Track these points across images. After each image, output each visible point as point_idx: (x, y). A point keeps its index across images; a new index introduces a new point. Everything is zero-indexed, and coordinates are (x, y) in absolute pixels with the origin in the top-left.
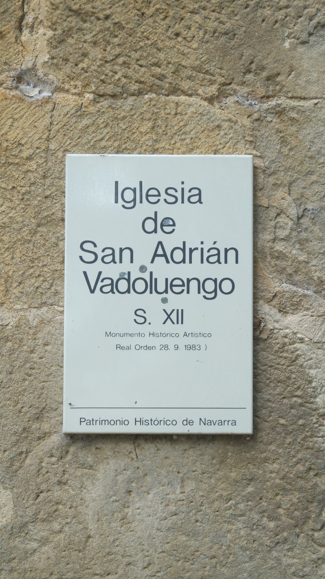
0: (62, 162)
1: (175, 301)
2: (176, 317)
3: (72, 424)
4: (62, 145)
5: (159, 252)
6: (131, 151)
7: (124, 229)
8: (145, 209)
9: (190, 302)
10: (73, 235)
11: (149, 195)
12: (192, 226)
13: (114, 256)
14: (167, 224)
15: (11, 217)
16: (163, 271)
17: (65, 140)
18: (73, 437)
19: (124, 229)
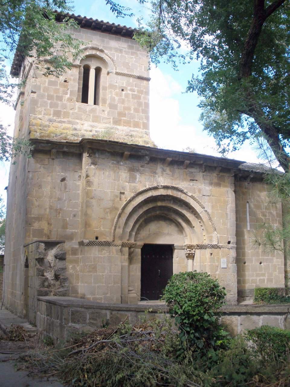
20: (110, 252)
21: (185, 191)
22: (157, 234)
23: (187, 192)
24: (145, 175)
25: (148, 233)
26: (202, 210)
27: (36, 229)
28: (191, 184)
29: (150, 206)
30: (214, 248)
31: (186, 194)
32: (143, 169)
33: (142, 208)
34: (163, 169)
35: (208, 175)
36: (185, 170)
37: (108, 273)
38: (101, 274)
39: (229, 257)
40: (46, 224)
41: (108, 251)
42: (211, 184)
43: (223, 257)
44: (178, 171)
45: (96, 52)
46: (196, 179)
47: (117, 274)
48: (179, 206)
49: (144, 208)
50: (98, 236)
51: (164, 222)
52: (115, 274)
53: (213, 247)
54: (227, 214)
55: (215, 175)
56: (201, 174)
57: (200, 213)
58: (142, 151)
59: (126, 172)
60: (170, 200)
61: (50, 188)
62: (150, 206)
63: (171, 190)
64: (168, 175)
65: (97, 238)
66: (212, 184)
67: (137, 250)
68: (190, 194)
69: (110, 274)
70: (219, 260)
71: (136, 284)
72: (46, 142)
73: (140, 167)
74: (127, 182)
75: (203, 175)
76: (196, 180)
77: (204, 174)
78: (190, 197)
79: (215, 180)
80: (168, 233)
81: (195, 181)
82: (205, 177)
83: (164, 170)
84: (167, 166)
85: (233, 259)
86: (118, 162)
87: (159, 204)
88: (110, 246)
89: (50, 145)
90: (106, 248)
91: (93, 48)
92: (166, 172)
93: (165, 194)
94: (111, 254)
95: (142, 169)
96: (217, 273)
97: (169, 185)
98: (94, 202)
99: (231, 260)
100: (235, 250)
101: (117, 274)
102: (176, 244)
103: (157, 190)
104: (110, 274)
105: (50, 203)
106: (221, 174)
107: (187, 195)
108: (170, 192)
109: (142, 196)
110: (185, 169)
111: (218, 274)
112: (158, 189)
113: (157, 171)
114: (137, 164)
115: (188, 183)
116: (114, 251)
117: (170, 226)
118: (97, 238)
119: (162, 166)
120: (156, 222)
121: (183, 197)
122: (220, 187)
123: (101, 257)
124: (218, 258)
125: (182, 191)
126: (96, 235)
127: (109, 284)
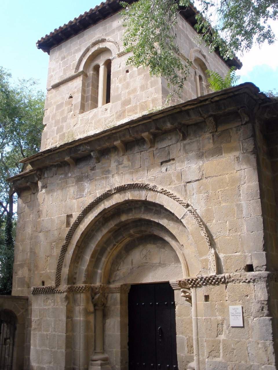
0: (229, 308)
1: (237, 317)
2: (237, 318)
3: (231, 326)
4: (58, 282)
5: (236, 313)
6: (71, 261)
7: (233, 311)
8: (235, 310)
9: (238, 317)
10: (230, 312)
11: (235, 309)
12: (238, 311)
13: (233, 313)
14: (236, 311)
15: (205, 341)
16: (236, 314)
17: (241, 15)
18: (232, 327)
19: (233, 311)
20: (54, 302)
21: (151, 185)
22: (144, 267)
23: (155, 186)
24: (96, 180)
25: (130, 266)
26: (186, 210)
27: (20, 278)
28: (164, 169)
29: (112, 224)
30: (211, 283)
31: (154, 191)
32: (93, 172)
33: (101, 231)
34: (118, 162)
35: (194, 142)
36: (152, 149)
37: (52, 332)
38: (45, 333)
39: (248, 301)
40: (27, 271)
41: (53, 301)
42: (201, 156)
43: (234, 302)
44: (140, 156)
45: (98, 46)
46: (171, 157)
47: (61, 334)
48: (155, 213)
49: (103, 229)
50: (44, 280)
51: (154, 244)
52: (59, 334)
53: (208, 281)
54: (239, 206)
55: (208, 135)
56: (180, 145)
57: (183, 218)
58: (81, 148)
59: (74, 184)
60: (140, 208)
61: (32, 228)
62: (112, 224)
63: (130, 191)
64: (126, 168)
65: (43, 283)
66: (203, 155)
67: (115, 295)
68: (159, 189)
69: (54, 333)
70: (224, 310)
71: (114, 350)
72: (19, 178)
73: (89, 171)
74: (74, 198)
75: (184, 147)
76: (173, 159)
77: (185, 142)
78: (161, 193)
79: (210, 145)
80: (160, 263)
81: (172, 162)
82: (187, 147)
83: (120, 163)
84: (123, 155)
85: (259, 305)
86: (66, 174)
87: (124, 218)
88: (55, 294)
89: (23, 179)
90: (50, 296)
91: (94, 44)
92: (123, 165)
93: (122, 200)
94: (56, 304)
95: (91, 173)
96: (222, 337)
97: (123, 184)
98: (41, 236)
99: (255, 307)
100: (264, 285)
101: (61, 334)
102: (173, 281)
103: (110, 197)
104: (54, 333)
105: (31, 245)
106: (220, 129)
107: (157, 191)
108: (129, 196)
109: (92, 213)
110: (151, 147)
111: (224, 340)
112: (112, 196)
113: (110, 169)
114: (85, 168)
115: (159, 169)
116: (59, 300)
117: (163, 250)
118: (43, 283)
119: (116, 157)
120: (141, 247)
121: (151, 197)
122: (222, 154)
123: (46, 308)
124: (222, 305)
125: (144, 187)
126: (42, 279)
127: (53, 348)
